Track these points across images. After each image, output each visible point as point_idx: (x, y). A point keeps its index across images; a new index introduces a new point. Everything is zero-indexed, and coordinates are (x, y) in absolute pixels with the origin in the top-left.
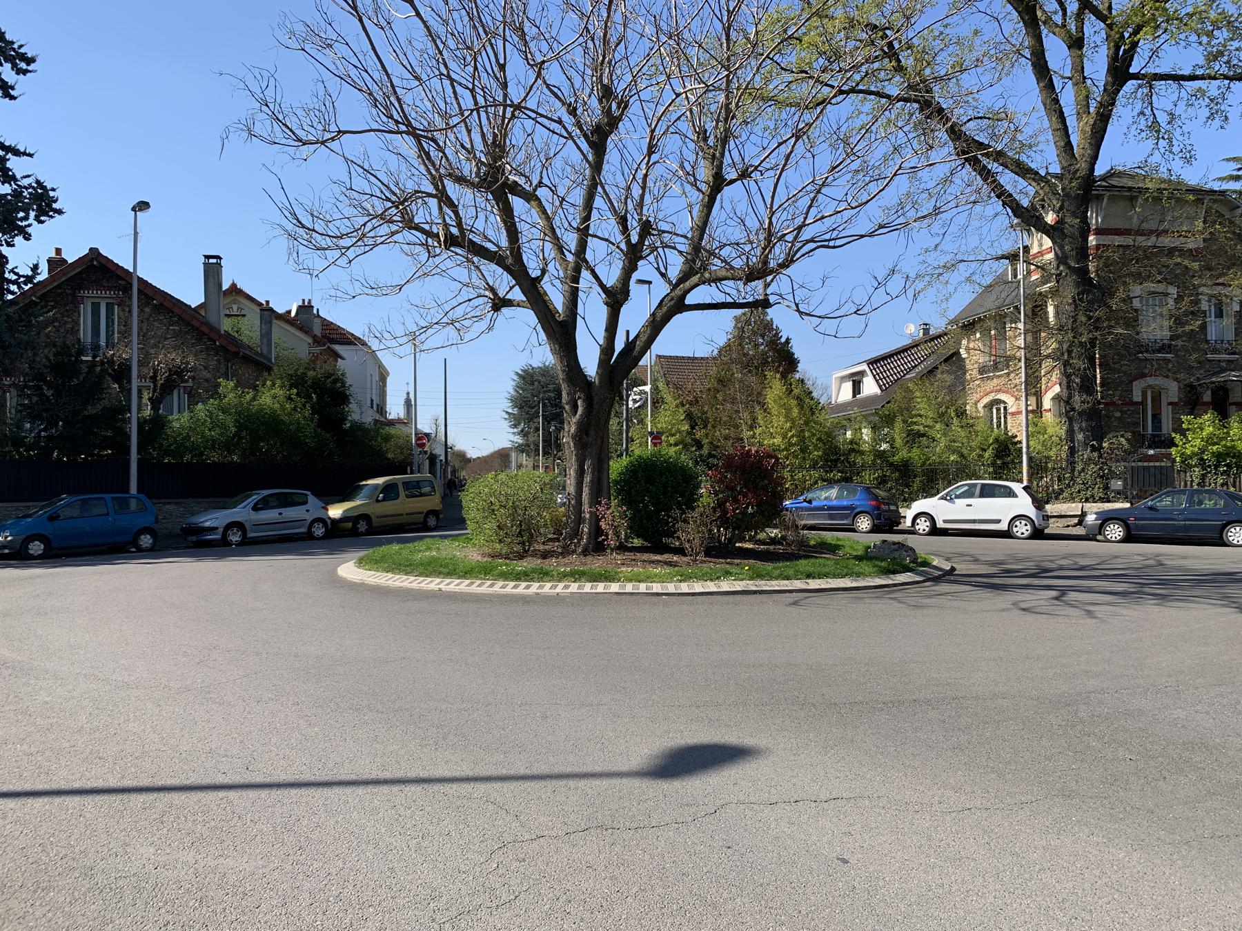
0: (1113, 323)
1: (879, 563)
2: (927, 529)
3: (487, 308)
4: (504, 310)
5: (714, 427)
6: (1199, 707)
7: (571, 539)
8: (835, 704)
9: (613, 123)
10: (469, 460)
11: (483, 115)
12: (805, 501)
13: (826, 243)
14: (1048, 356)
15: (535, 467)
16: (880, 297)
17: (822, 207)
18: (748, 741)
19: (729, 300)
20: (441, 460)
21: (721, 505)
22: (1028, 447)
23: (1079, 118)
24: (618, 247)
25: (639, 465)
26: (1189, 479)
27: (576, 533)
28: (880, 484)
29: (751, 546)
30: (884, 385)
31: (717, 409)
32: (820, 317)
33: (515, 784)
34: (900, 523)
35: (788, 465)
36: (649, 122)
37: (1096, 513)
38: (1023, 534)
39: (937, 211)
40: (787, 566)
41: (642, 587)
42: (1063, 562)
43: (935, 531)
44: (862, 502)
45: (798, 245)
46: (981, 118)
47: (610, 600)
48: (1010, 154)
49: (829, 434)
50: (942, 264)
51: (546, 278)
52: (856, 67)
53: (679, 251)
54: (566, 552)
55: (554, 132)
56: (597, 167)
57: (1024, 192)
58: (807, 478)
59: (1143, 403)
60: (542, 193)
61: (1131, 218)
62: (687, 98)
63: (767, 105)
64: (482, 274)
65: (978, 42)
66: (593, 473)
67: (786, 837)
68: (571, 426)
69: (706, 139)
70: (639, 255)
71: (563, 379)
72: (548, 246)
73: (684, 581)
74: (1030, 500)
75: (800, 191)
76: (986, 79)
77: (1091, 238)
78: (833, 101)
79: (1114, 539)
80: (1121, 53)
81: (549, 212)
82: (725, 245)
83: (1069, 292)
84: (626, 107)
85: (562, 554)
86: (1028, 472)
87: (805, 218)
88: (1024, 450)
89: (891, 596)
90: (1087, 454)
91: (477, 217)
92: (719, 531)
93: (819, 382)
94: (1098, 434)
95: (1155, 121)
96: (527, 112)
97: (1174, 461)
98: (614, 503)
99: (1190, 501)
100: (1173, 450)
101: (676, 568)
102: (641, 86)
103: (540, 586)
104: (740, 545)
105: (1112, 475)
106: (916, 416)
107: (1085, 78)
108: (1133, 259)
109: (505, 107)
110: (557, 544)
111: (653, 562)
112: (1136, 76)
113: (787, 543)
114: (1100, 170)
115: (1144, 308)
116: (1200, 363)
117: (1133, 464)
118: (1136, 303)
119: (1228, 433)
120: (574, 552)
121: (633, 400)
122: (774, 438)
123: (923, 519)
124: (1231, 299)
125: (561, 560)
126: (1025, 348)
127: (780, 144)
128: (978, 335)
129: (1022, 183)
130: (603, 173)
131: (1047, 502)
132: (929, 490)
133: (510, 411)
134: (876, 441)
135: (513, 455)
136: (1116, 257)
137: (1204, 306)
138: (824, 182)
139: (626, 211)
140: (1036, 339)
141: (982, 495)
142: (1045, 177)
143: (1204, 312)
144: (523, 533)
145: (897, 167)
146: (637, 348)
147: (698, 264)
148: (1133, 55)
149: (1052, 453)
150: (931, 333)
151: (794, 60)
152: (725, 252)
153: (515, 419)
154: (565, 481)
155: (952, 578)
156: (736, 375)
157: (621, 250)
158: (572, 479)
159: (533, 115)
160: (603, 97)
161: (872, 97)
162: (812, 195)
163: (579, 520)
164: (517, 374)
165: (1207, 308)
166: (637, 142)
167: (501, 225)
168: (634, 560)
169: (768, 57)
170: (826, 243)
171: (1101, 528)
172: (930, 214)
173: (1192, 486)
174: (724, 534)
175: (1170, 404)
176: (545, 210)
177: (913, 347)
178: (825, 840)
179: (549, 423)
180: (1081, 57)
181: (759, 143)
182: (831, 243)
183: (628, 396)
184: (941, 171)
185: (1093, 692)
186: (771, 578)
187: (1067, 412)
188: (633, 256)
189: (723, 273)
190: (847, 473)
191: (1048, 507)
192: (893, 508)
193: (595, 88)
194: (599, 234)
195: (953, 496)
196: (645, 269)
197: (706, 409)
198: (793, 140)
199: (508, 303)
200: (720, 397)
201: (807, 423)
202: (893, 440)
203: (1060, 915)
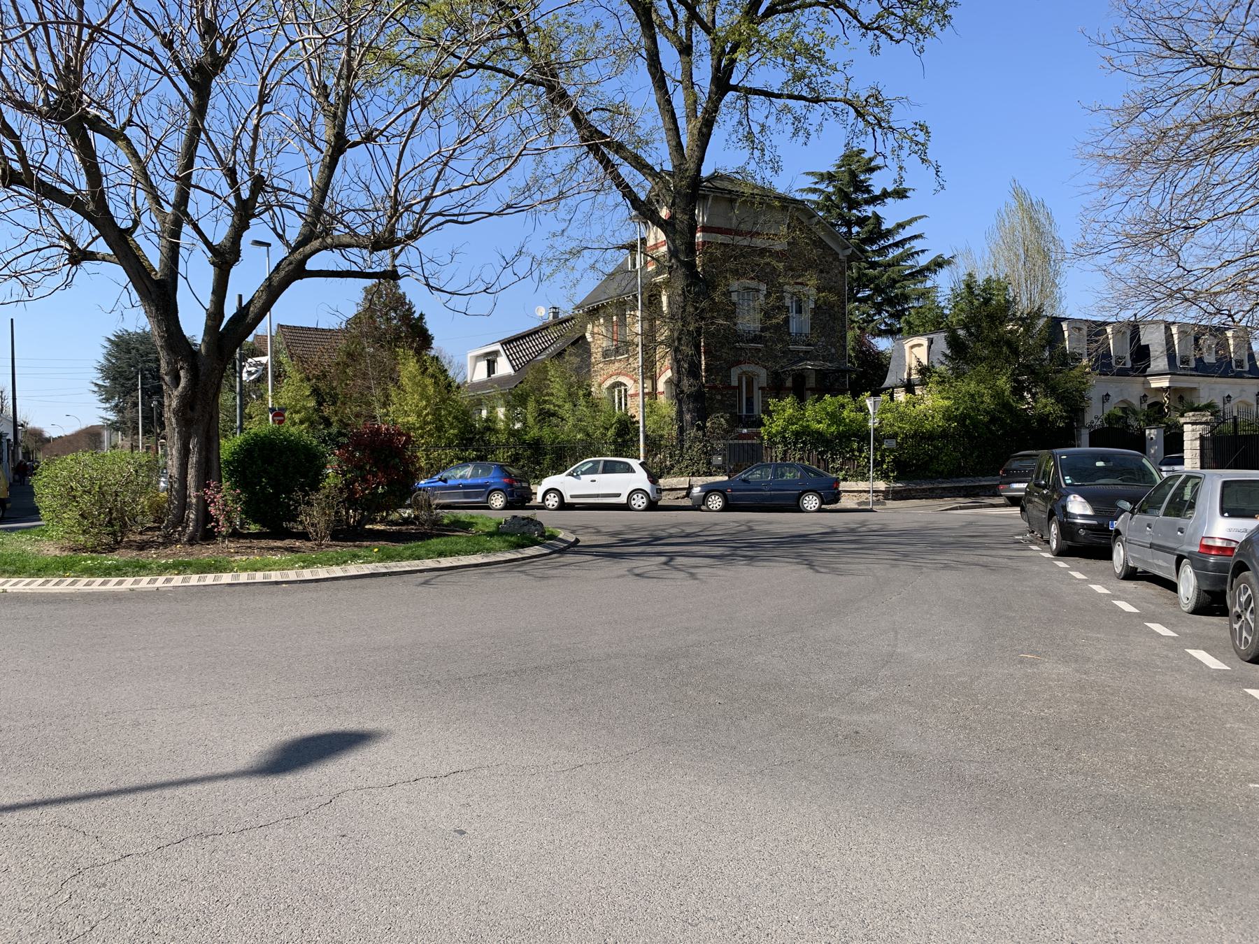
0: (715, 314)
1: (509, 538)
2: (556, 504)
3: (63, 260)
4: (86, 264)
5: (344, 403)
6: (775, 653)
7: (175, 527)
8: (460, 679)
9: (218, 64)
10: (48, 440)
11: (52, 33)
12: (440, 480)
13: (455, 218)
14: (661, 343)
15: (134, 447)
16: (507, 277)
17: (449, 181)
18: (369, 726)
19: (355, 268)
20: (9, 440)
21: (349, 484)
22: (644, 426)
23: (688, 122)
24: (225, 201)
25: (256, 444)
26: (774, 454)
27: (181, 520)
28: (513, 462)
29: (383, 528)
30: (517, 365)
31: (346, 384)
32: (450, 293)
33: (96, 802)
34: (531, 499)
35: (423, 444)
36: (260, 69)
37: (700, 486)
38: (639, 506)
39: (561, 196)
40: (419, 546)
41: (259, 577)
42: (672, 531)
43: (563, 506)
44: (496, 480)
45: (426, 217)
46: (602, 109)
47: (221, 592)
48: (629, 148)
49: (465, 413)
50: (568, 250)
51: (139, 230)
52: (483, 42)
53: (299, 213)
54: (168, 541)
55: (146, 65)
56: (200, 110)
57: (642, 186)
58: (443, 457)
59: (739, 387)
60: (132, 133)
61: (731, 219)
62: (304, 47)
63: (394, 69)
64: (56, 221)
65: (599, 34)
66: (200, 452)
67: (404, 818)
68: (172, 400)
69: (327, 96)
70: (250, 212)
71: (161, 346)
72: (141, 195)
73: (307, 567)
74: (645, 475)
75: (426, 161)
76: (605, 72)
77: (698, 235)
78: (463, 74)
79: (714, 509)
80: (723, 65)
81: (142, 156)
82: (349, 210)
83: (679, 284)
84: (233, 48)
85: (162, 544)
86: (644, 449)
87: (433, 190)
88: (641, 429)
89: (519, 569)
90: (693, 432)
91: (47, 153)
92: (347, 513)
93: (455, 360)
94: (702, 414)
95: (750, 133)
96: (110, 37)
97: (763, 439)
98: (226, 485)
99: (775, 474)
100: (762, 430)
101: (298, 555)
102: (250, 28)
103: (135, 581)
104: (371, 526)
105: (714, 451)
106: (548, 394)
107: (693, 84)
108: (732, 257)
109: (81, 27)
110: (157, 533)
111: (272, 549)
112: (735, 88)
113: (420, 523)
114: (706, 172)
115: (741, 302)
116: (783, 353)
117: (731, 442)
118: (734, 297)
119: (804, 414)
120: (178, 541)
121: (248, 372)
122: (409, 416)
123: (552, 495)
124: (808, 298)
125: (161, 550)
126: (642, 335)
127: (406, 111)
128: (602, 321)
129: (640, 177)
130: (208, 118)
131: (660, 477)
132: (558, 467)
133: (101, 383)
134: (510, 419)
135: (106, 434)
136: (718, 253)
137: (788, 302)
138: (452, 155)
139: (235, 162)
140: (652, 326)
141: (605, 471)
142: (659, 173)
143: (788, 308)
144: (114, 522)
145: (522, 147)
146: (251, 315)
147: (319, 227)
148: (732, 68)
149: (665, 433)
150: (560, 317)
151: (422, 26)
152: (348, 218)
153: (107, 392)
154: (166, 463)
155: (576, 549)
156: (367, 350)
157: (229, 204)
158: (174, 459)
159: (118, 42)
160: (206, 32)
161: (501, 75)
162: (440, 167)
163: (184, 505)
164: (109, 340)
165: (790, 305)
166: (247, 89)
167: (80, 165)
168: (250, 547)
169: (391, 16)
170: (455, 218)
171: (704, 499)
172: (555, 198)
173: (776, 461)
174: (353, 516)
175: (760, 388)
176: (136, 152)
177: (543, 329)
178: (443, 814)
179: (150, 397)
180: (690, 63)
181: (384, 107)
182: (460, 219)
183: (242, 367)
184: (567, 157)
185: (692, 646)
186: (402, 559)
187: (677, 395)
188: (244, 213)
189: (347, 240)
190: (481, 451)
191: (661, 481)
192: (524, 485)
193: (195, 21)
194: (202, 185)
195: (579, 473)
196: (258, 229)
197: (334, 385)
198: (419, 108)
199: (91, 256)
200: (350, 371)
201: (443, 401)
202: (525, 419)
203: (655, 852)
